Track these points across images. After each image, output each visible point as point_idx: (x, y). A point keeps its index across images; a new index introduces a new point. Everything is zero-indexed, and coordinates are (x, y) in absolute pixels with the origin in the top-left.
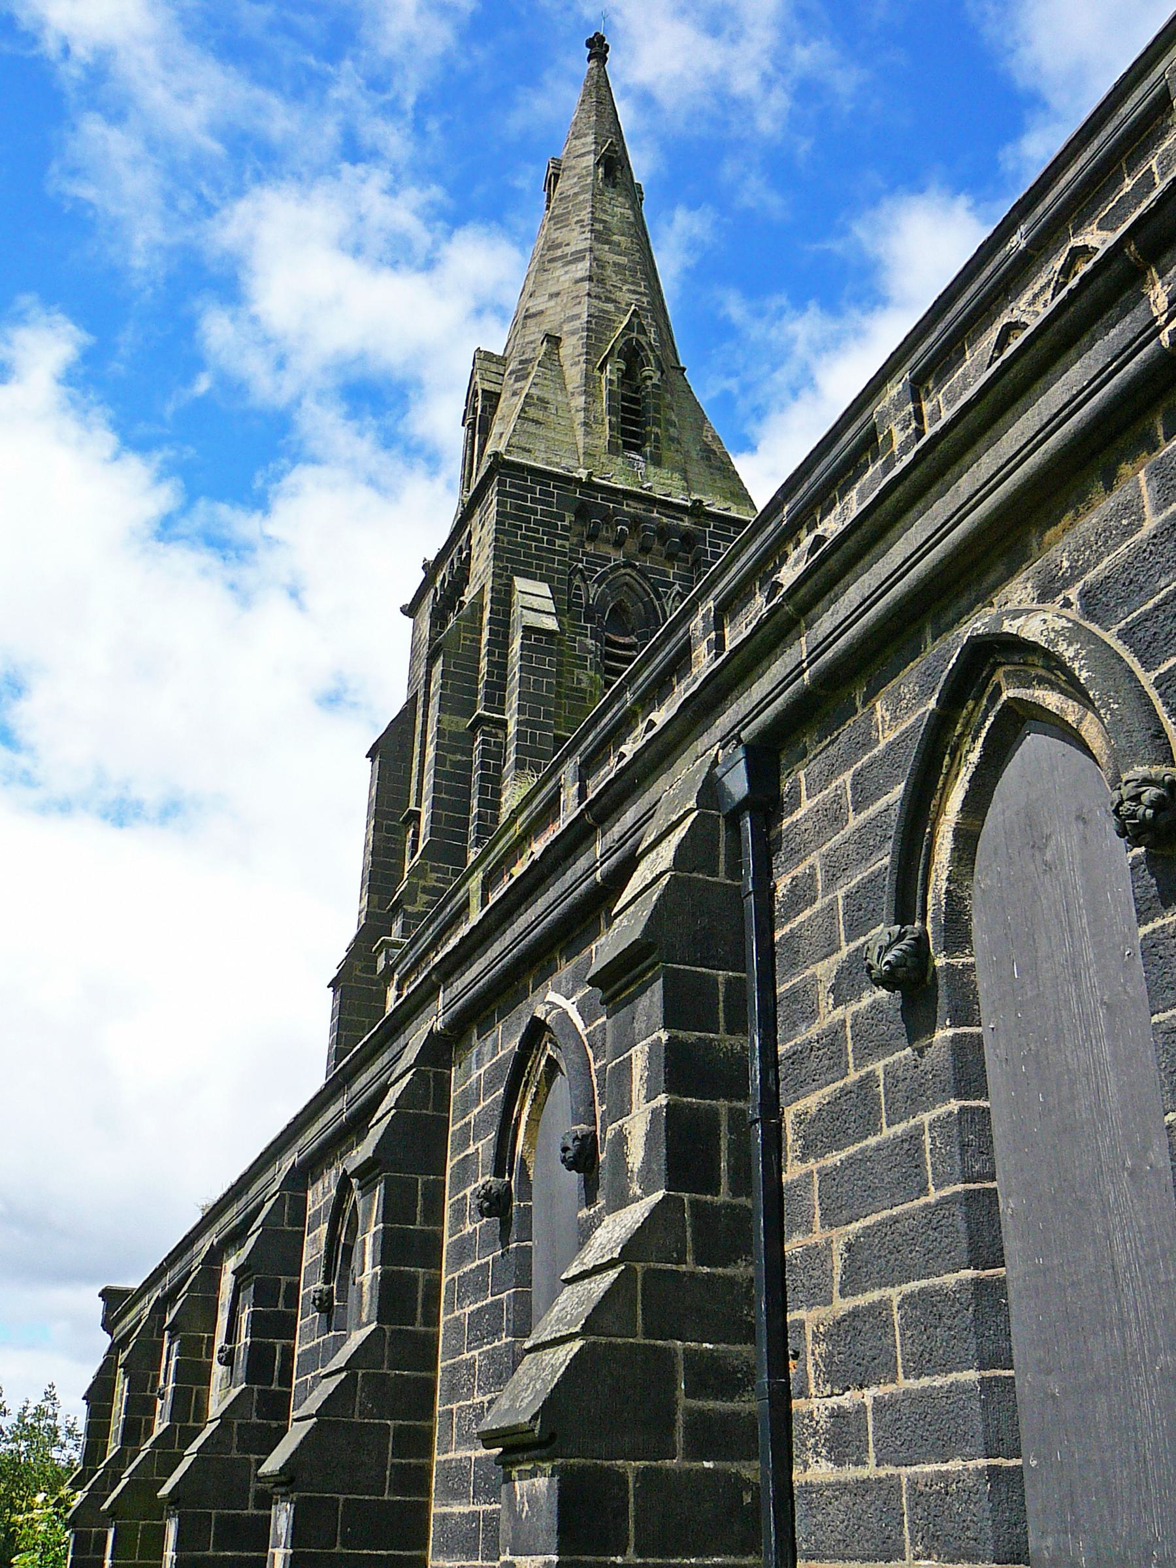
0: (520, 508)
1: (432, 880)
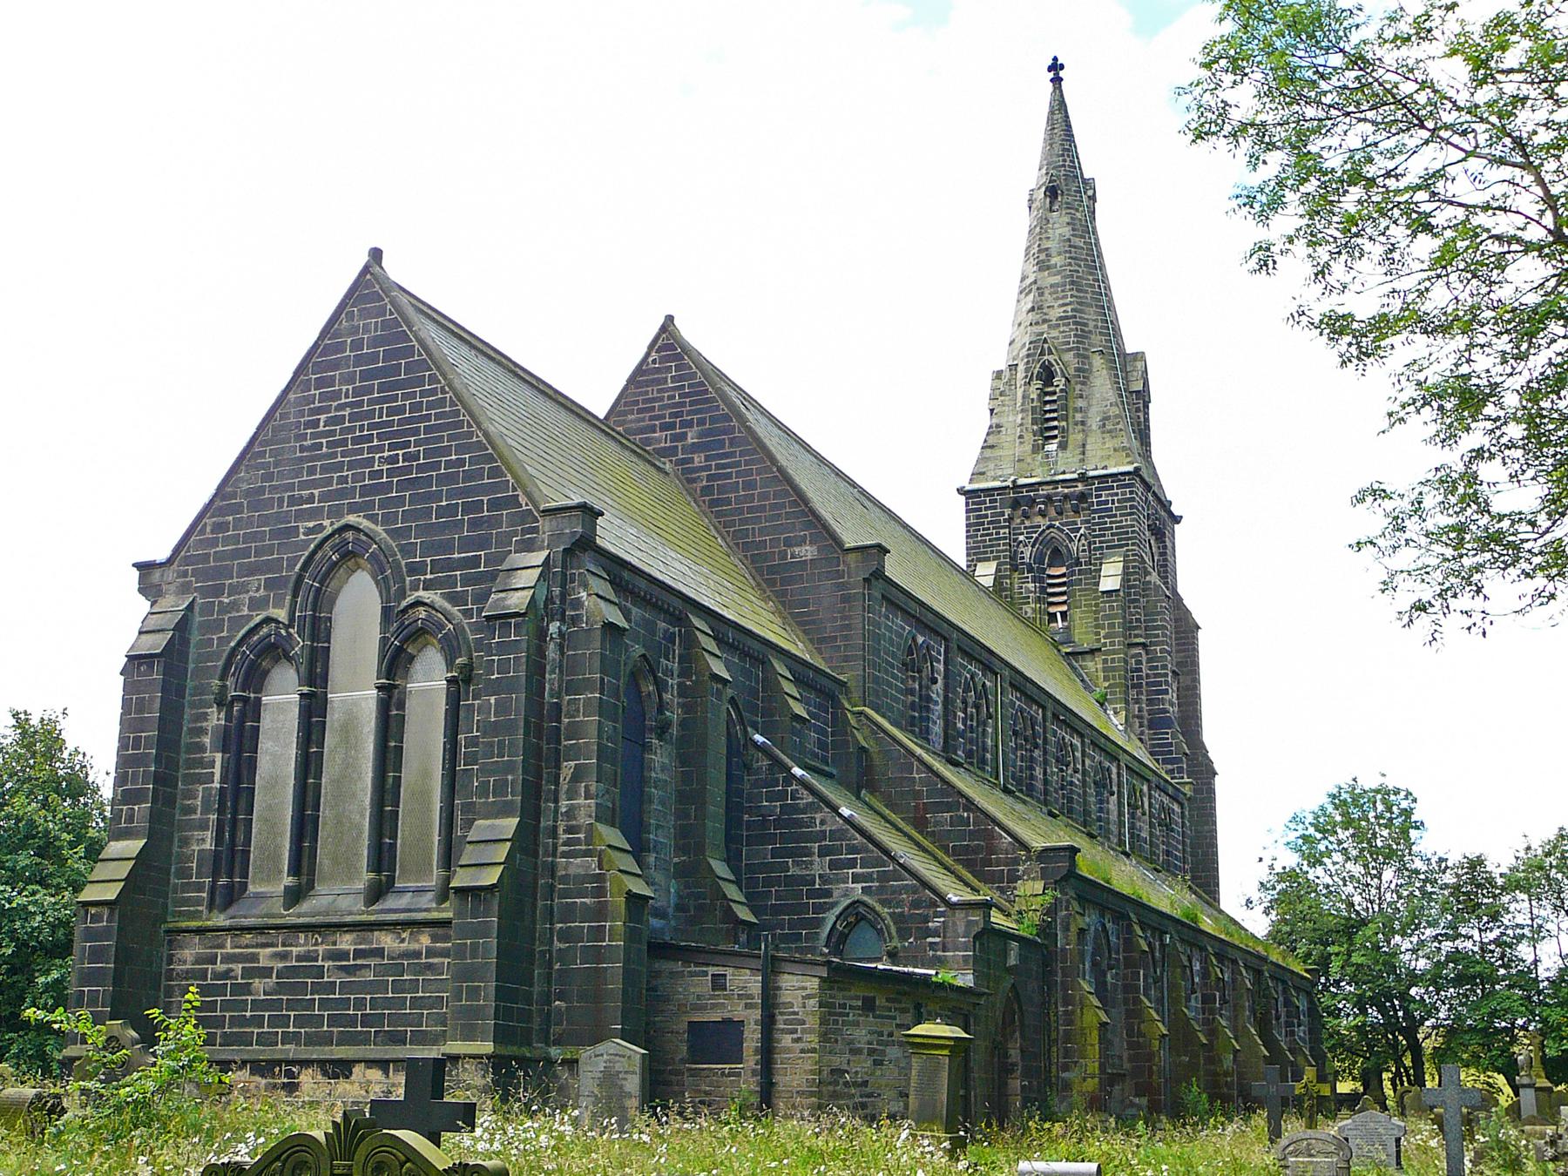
0: (978, 517)
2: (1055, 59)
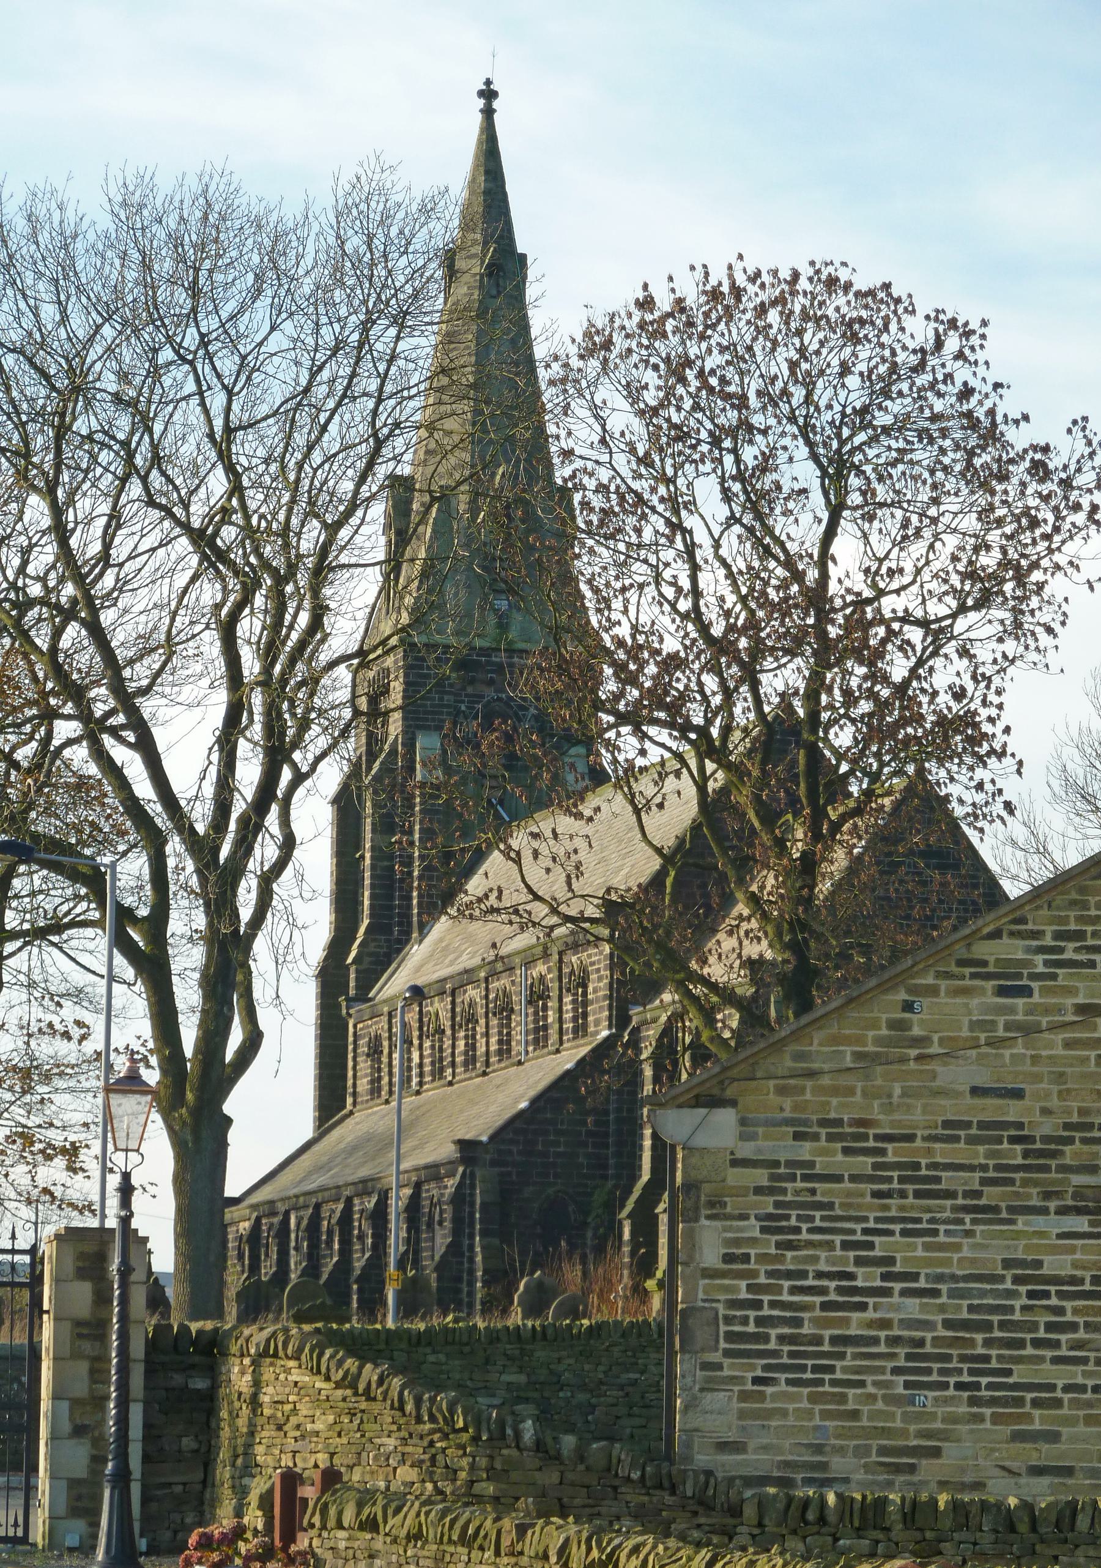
1: (372, 947)
2: (488, 82)
